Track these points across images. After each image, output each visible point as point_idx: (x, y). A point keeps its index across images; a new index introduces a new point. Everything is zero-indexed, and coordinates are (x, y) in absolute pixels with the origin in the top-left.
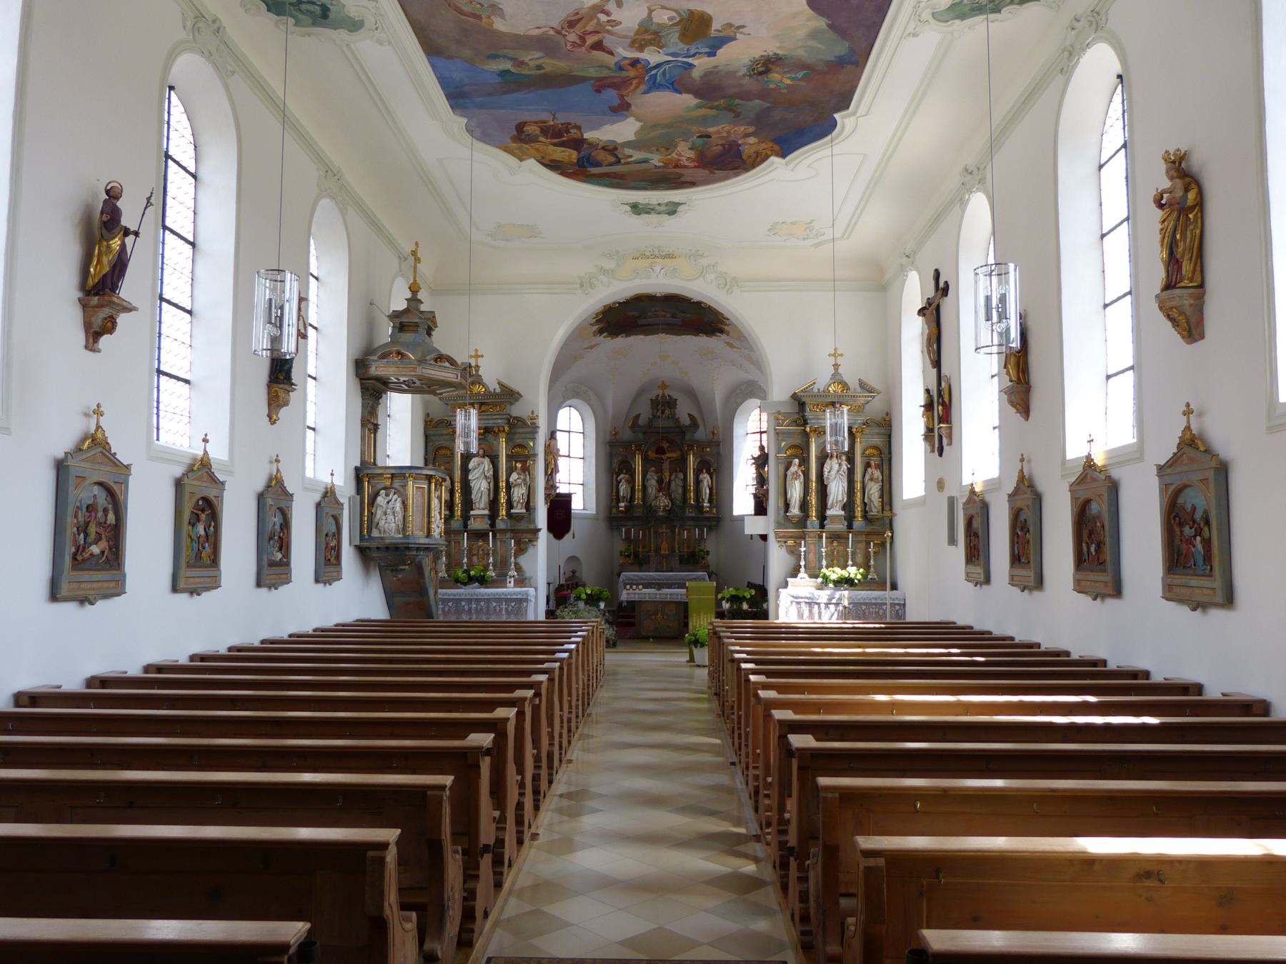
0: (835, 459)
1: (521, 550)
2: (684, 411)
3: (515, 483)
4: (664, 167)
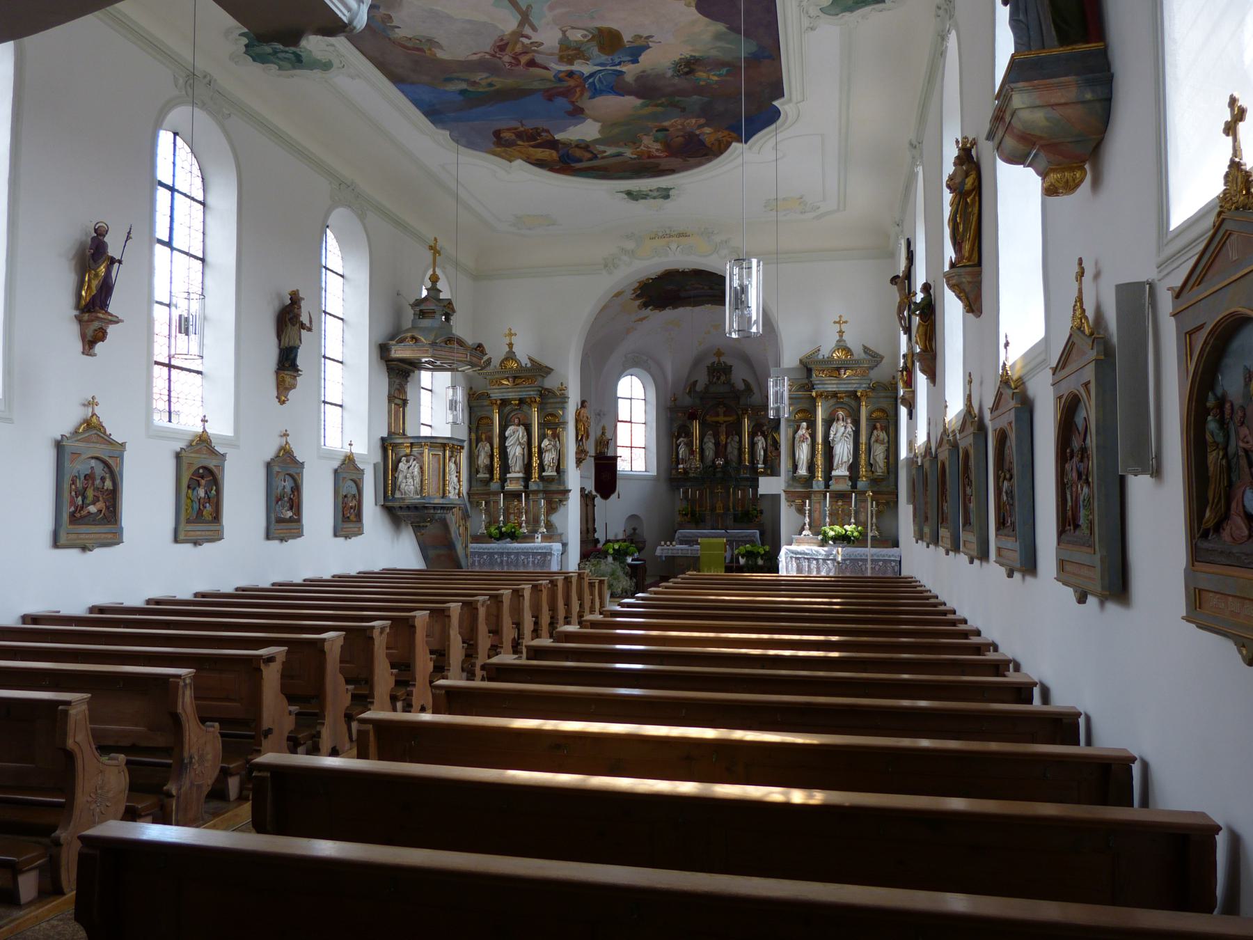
0: (841, 422)
1: (552, 508)
3: (545, 448)
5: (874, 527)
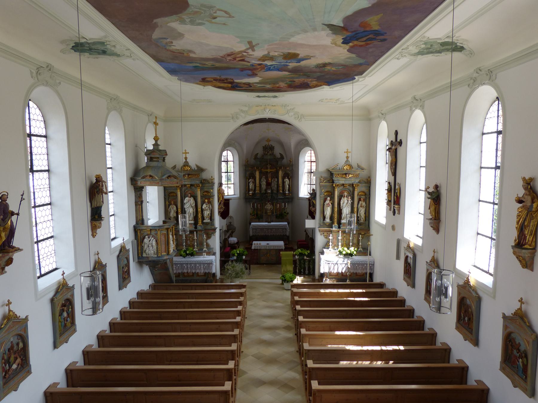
0: (346, 197)
1: (209, 237)
2: (278, 151)
4: (272, 88)
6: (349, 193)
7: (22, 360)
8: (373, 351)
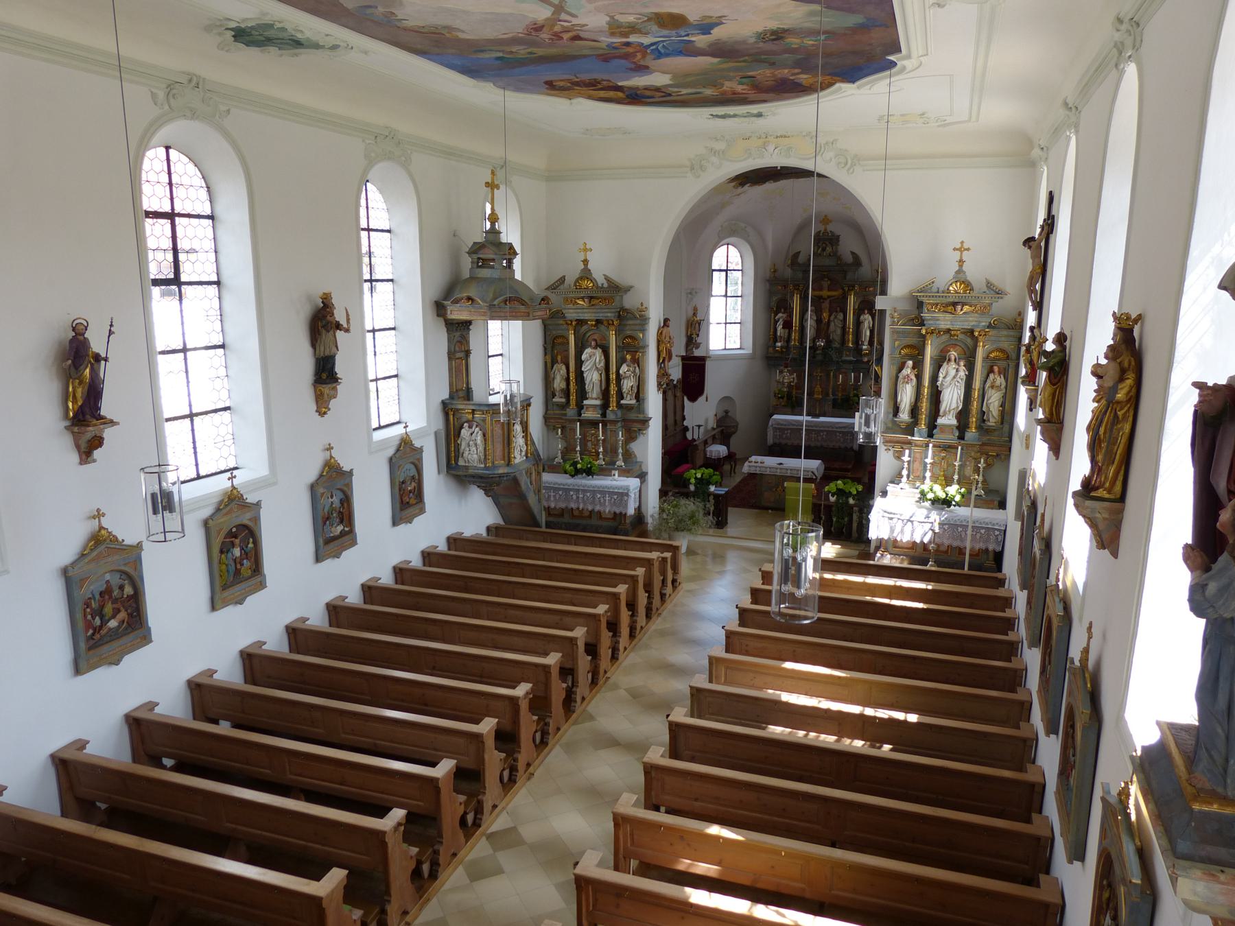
0: (953, 363)
1: (631, 436)
5: (980, 485)
6: (964, 351)
7: (130, 615)
8: (840, 713)
